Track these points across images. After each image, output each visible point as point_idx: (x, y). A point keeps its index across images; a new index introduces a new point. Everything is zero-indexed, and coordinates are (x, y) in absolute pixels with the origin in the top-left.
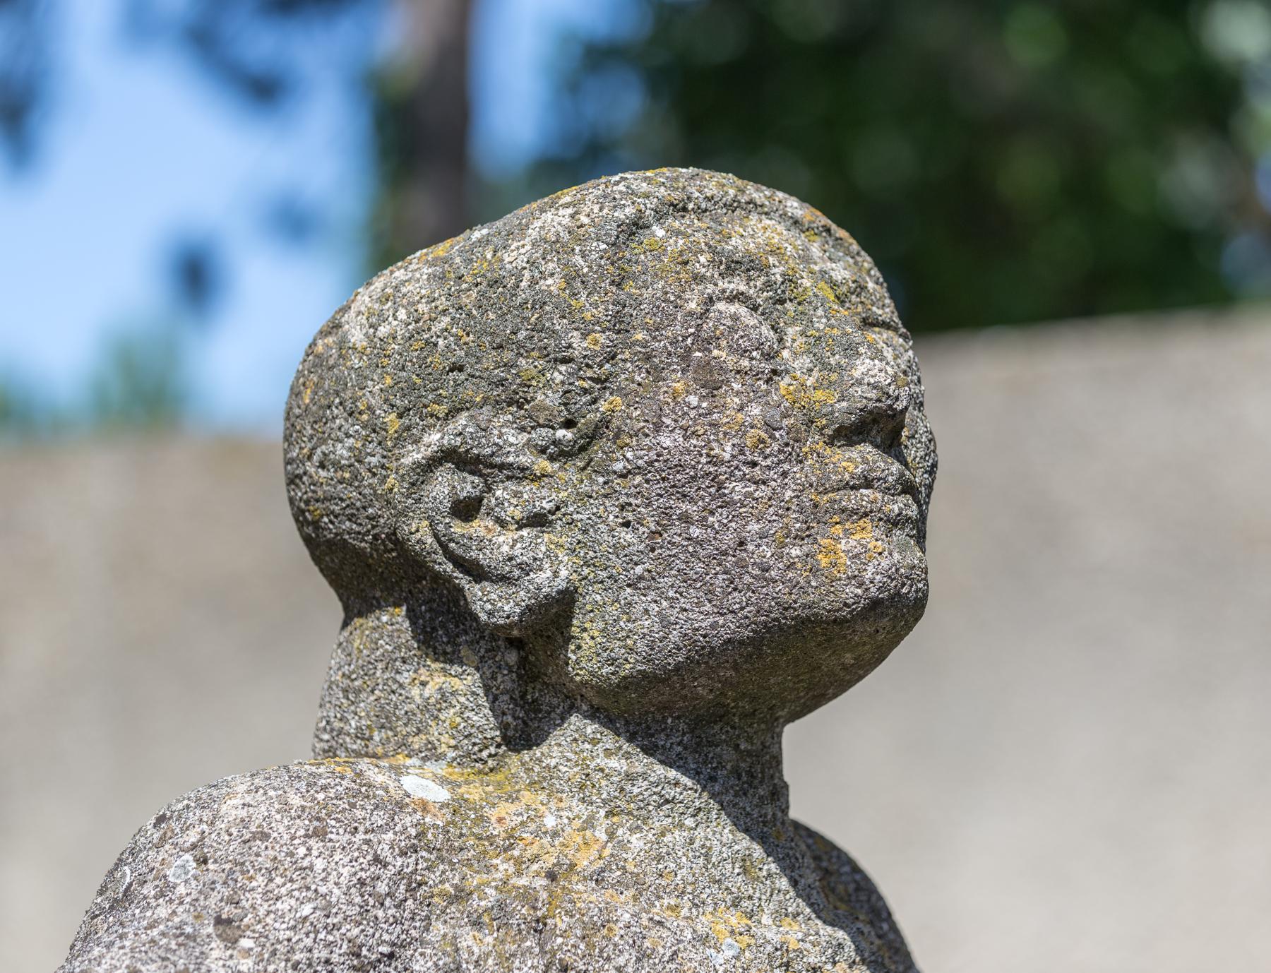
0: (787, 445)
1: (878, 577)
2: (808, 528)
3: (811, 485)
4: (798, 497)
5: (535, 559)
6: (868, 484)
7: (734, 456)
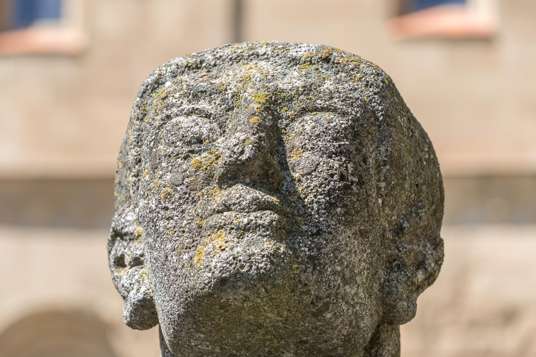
0: (186, 193)
1: (219, 265)
2: (194, 241)
3: (198, 215)
4: (189, 223)
5: (131, 284)
6: (228, 208)
7: (157, 206)
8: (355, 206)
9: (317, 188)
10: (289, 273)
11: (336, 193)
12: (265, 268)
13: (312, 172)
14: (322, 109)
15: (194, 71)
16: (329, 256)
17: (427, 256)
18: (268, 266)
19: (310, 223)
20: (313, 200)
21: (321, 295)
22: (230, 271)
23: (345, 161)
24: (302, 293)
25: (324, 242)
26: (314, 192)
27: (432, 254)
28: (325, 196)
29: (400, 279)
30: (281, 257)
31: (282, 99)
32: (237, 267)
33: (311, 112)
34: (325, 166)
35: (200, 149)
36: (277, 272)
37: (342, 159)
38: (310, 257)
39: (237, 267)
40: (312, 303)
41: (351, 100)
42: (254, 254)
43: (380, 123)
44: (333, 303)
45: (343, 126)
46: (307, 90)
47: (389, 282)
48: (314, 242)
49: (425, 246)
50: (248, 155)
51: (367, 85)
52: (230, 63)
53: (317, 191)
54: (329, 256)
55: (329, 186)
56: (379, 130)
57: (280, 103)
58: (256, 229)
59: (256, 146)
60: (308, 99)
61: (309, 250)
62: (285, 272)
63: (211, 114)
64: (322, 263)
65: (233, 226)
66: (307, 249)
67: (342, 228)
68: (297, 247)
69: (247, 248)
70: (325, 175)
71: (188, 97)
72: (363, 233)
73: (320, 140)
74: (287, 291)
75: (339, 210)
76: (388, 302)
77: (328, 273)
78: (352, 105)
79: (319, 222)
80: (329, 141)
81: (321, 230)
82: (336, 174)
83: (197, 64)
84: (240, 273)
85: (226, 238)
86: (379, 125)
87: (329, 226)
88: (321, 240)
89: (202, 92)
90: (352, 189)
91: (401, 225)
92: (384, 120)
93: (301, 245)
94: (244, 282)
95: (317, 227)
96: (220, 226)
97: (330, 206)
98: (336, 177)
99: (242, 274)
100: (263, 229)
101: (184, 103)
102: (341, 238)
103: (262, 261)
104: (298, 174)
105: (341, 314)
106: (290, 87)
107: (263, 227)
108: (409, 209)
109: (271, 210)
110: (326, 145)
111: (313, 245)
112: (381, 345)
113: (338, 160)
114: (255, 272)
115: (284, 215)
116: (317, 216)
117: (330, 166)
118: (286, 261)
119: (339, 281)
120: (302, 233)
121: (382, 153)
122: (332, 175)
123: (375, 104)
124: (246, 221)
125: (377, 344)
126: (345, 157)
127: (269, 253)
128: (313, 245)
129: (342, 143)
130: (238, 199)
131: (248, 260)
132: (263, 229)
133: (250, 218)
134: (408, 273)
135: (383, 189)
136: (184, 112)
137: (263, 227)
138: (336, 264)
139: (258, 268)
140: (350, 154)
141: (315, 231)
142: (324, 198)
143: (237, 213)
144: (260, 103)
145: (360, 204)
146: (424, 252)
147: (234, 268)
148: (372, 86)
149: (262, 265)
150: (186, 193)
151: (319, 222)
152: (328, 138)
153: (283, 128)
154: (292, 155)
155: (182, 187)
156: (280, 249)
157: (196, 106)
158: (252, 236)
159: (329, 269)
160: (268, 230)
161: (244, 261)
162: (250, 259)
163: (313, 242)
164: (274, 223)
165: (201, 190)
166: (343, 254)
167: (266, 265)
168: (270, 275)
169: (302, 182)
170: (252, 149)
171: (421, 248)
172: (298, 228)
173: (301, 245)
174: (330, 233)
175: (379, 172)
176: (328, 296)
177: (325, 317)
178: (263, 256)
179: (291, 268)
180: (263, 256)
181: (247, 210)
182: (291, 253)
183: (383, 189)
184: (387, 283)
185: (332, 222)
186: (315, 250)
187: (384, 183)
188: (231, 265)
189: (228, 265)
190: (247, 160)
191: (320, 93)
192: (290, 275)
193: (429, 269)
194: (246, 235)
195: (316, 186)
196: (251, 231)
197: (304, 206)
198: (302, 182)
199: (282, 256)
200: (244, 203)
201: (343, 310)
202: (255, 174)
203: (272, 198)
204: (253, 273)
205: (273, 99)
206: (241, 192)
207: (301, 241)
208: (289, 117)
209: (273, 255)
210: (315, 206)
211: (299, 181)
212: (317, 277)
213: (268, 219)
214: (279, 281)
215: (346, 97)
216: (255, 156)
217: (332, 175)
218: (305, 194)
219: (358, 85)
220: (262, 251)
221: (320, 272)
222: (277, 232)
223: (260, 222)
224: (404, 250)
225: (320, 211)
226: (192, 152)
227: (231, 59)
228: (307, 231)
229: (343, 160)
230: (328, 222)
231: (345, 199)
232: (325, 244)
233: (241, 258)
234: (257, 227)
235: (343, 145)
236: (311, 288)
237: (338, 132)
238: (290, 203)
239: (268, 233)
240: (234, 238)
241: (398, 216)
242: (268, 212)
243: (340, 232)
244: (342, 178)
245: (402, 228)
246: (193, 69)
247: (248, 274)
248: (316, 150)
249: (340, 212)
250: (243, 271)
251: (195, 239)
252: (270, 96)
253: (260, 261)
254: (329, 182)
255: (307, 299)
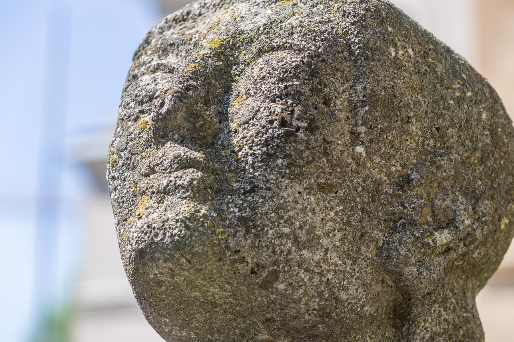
1: (135, 235)
8: (304, 156)
9: (253, 138)
10: (211, 239)
11: (274, 142)
12: (179, 235)
13: (250, 120)
14: (279, 48)
15: (180, 23)
16: (269, 216)
17: (457, 212)
18: (183, 232)
19: (243, 179)
20: (248, 152)
21: (262, 262)
22: (145, 241)
23: (292, 104)
24: (234, 262)
25: (261, 200)
26: (250, 144)
27: (465, 210)
28: (262, 147)
29: (405, 241)
30: (199, 220)
31: (242, 42)
32: (151, 236)
33: (268, 52)
34: (265, 111)
35: (150, 107)
36: (194, 238)
37: (287, 102)
38: (241, 219)
39: (151, 236)
40: (253, 272)
41: (314, 34)
42: (168, 219)
43: (356, 57)
44: (284, 272)
45: (294, 64)
46: (268, 27)
47: (388, 244)
48: (246, 201)
49: (455, 201)
50: (167, 107)
51: (344, 16)
52: (214, 9)
53: (253, 142)
54: (269, 216)
55: (266, 134)
56: (355, 66)
57: (239, 46)
58: (175, 190)
59: (176, 96)
60: (267, 38)
61: (239, 211)
62: (204, 238)
63: (174, 68)
64: (258, 226)
65: (154, 190)
66: (236, 210)
67: (287, 182)
68: (225, 208)
69: (163, 213)
70: (263, 122)
71: (159, 52)
72: (323, 188)
73: (265, 83)
74: (211, 259)
75: (279, 161)
76: (390, 269)
77: (269, 236)
78: (315, 40)
79: (254, 177)
80: (274, 83)
81: (257, 187)
82: (276, 120)
83: (183, 16)
84: (154, 242)
85: (147, 204)
86: (354, 60)
87: (267, 181)
88: (256, 198)
89: (171, 45)
90: (297, 136)
91: (408, 176)
92: (362, 54)
93: (230, 205)
94: (161, 252)
95: (251, 183)
96: (143, 192)
97: (268, 158)
98: (276, 124)
99: (157, 243)
100: (182, 190)
101: (154, 59)
102: (285, 195)
103: (176, 227)
104: (235, 124)
105: (300, 284)
106: (252, 27)
107: (183, 188)
108: (424, 157)
109: (193, 167)
110: (270, 87)
111: (245, 205)
112: (413, 322)
113: (282, 104)
114: (169, 239)
115: (213, 173)
116: (251, 170)
117: (271, 112)
118: (206, 224)
119: (290, 245)
120: (233, 192)
121: (359, 92)
122: (271, 122)
123: (351, 36)
124: (165, 182)
125: (409, 320)
126: (293, 99)
127: (184, 217)
128: (245, 205)
129: (288, 84)
130: (160, 158)
131: (162, 227)
132: (182, 190)
133: (170, 179)
134: (415, 233)
135: (363, 135)
136: (150, 70)
137: (183, 188)
138: (281, 226)
139: (172, 236)
140: (299, 96)
141: (249, 188)
142: (260, 149)
143: (160, 174)
144: (210, 49)
145: (311, 153)
146: (454, 208)
147: (149, 237)
148: (350, 16)
149: (175, 232)
150: (127, 159)
151: (254, 177)
152: (273, 80)
153: (237, 75)
154: (234, 104)
155: (125, 152)
156: (200, 212)
157: (164, 62)
158: (172, 199)
159: (270, 232)
160: (188, 191)
161: (158, 229)
162: (163, 226)
163: (245, 201)
164: (195, 182)
165: (142, 153)
166: (291, 213)
167: (180, 231)
168: (185, 242)
169: (238, 133)
170: (171, 100)
171: (448, 202)
172: (227, 185)
173: (230, 205)
174: (269, 189)
175: (356, 114)
176: (275, 263)
177: (277, 288)
178: (177, 221)
179: (214, 232)
180: (177, 221)
181: (168, 170)
182: (215, 215)
183: (363, 135)
184: (386, 246)
185: (272, 176)
186: (247, 210)
187: (364, 127)
188: (146, 233)
189: (143, 234)
190: (166, 112)
191: (280, 29)
192: (213, 240)
193: (461, 228)
194: (166, 198)
195: (253, 135)
196: (171, 194)
197: (237, 160)
198: (238, 133)
199: (201, 220)
200: (166, 163)
201: (303, 279)
202: (184, 128)
203: (196, 153)
204: (167, 241)
205: (231, 43)
206: (172, 150)
207: (231, 200)
208: (245, 61)
209: (190, 219)
210: (250, 159)
211: (236, 132)
212: (252, 242)
213: (188, 179)
214: (197, 249)
215: (309, 31)
216: (175, 107)
217: (271, 122)
218: (240, 146)
219: (334, 16)
220: (177, 215)
221: (257, 236)
222: (197, 192)
223: (179, 182)
224: (412, 205)
225: (256, 165)
226: (142, 112)
227: (214, 5)
228: (239, 188)
229: (289, 104)
230: (266, 177)
231: (287, 148)
232: (262, 202)
233: (155, 225)
234: (176, 188)
235: (290, 85)
236: (245, 255)
237: (287, 72)
238: (220, 159)
239: (188, 194)
240: (154, 203)
241: (404, 166)
242: (191, 170)
243: (284, 187)
244: (283, 123)
245: (409, 179)
246: (180, 21)
247: (163, 243)
248: (259, 95)
249: (282, 164)
250: (157, 240)
251: (130, 209)
252: (228, 40)
253: (174, 227)
254: (267, 130)
255: (243, 269)
